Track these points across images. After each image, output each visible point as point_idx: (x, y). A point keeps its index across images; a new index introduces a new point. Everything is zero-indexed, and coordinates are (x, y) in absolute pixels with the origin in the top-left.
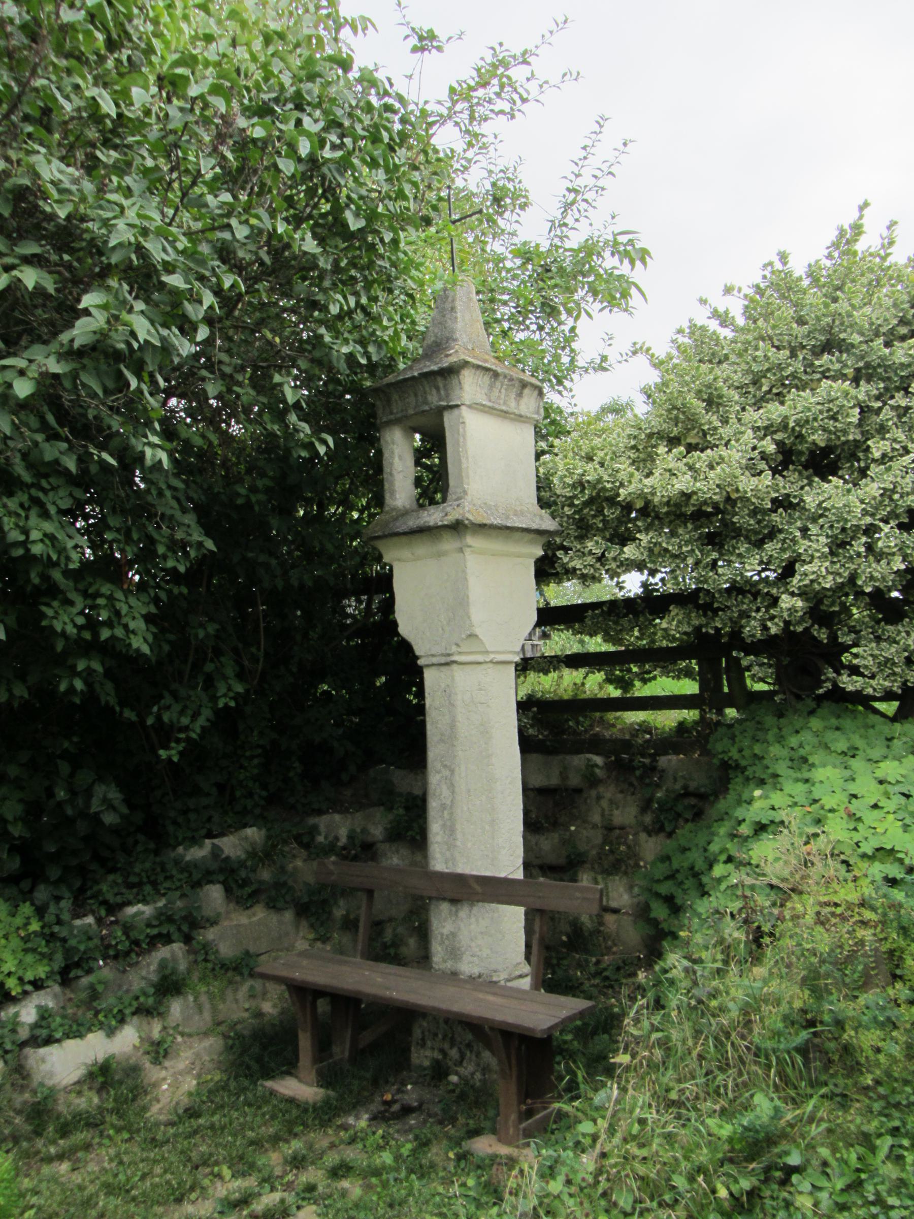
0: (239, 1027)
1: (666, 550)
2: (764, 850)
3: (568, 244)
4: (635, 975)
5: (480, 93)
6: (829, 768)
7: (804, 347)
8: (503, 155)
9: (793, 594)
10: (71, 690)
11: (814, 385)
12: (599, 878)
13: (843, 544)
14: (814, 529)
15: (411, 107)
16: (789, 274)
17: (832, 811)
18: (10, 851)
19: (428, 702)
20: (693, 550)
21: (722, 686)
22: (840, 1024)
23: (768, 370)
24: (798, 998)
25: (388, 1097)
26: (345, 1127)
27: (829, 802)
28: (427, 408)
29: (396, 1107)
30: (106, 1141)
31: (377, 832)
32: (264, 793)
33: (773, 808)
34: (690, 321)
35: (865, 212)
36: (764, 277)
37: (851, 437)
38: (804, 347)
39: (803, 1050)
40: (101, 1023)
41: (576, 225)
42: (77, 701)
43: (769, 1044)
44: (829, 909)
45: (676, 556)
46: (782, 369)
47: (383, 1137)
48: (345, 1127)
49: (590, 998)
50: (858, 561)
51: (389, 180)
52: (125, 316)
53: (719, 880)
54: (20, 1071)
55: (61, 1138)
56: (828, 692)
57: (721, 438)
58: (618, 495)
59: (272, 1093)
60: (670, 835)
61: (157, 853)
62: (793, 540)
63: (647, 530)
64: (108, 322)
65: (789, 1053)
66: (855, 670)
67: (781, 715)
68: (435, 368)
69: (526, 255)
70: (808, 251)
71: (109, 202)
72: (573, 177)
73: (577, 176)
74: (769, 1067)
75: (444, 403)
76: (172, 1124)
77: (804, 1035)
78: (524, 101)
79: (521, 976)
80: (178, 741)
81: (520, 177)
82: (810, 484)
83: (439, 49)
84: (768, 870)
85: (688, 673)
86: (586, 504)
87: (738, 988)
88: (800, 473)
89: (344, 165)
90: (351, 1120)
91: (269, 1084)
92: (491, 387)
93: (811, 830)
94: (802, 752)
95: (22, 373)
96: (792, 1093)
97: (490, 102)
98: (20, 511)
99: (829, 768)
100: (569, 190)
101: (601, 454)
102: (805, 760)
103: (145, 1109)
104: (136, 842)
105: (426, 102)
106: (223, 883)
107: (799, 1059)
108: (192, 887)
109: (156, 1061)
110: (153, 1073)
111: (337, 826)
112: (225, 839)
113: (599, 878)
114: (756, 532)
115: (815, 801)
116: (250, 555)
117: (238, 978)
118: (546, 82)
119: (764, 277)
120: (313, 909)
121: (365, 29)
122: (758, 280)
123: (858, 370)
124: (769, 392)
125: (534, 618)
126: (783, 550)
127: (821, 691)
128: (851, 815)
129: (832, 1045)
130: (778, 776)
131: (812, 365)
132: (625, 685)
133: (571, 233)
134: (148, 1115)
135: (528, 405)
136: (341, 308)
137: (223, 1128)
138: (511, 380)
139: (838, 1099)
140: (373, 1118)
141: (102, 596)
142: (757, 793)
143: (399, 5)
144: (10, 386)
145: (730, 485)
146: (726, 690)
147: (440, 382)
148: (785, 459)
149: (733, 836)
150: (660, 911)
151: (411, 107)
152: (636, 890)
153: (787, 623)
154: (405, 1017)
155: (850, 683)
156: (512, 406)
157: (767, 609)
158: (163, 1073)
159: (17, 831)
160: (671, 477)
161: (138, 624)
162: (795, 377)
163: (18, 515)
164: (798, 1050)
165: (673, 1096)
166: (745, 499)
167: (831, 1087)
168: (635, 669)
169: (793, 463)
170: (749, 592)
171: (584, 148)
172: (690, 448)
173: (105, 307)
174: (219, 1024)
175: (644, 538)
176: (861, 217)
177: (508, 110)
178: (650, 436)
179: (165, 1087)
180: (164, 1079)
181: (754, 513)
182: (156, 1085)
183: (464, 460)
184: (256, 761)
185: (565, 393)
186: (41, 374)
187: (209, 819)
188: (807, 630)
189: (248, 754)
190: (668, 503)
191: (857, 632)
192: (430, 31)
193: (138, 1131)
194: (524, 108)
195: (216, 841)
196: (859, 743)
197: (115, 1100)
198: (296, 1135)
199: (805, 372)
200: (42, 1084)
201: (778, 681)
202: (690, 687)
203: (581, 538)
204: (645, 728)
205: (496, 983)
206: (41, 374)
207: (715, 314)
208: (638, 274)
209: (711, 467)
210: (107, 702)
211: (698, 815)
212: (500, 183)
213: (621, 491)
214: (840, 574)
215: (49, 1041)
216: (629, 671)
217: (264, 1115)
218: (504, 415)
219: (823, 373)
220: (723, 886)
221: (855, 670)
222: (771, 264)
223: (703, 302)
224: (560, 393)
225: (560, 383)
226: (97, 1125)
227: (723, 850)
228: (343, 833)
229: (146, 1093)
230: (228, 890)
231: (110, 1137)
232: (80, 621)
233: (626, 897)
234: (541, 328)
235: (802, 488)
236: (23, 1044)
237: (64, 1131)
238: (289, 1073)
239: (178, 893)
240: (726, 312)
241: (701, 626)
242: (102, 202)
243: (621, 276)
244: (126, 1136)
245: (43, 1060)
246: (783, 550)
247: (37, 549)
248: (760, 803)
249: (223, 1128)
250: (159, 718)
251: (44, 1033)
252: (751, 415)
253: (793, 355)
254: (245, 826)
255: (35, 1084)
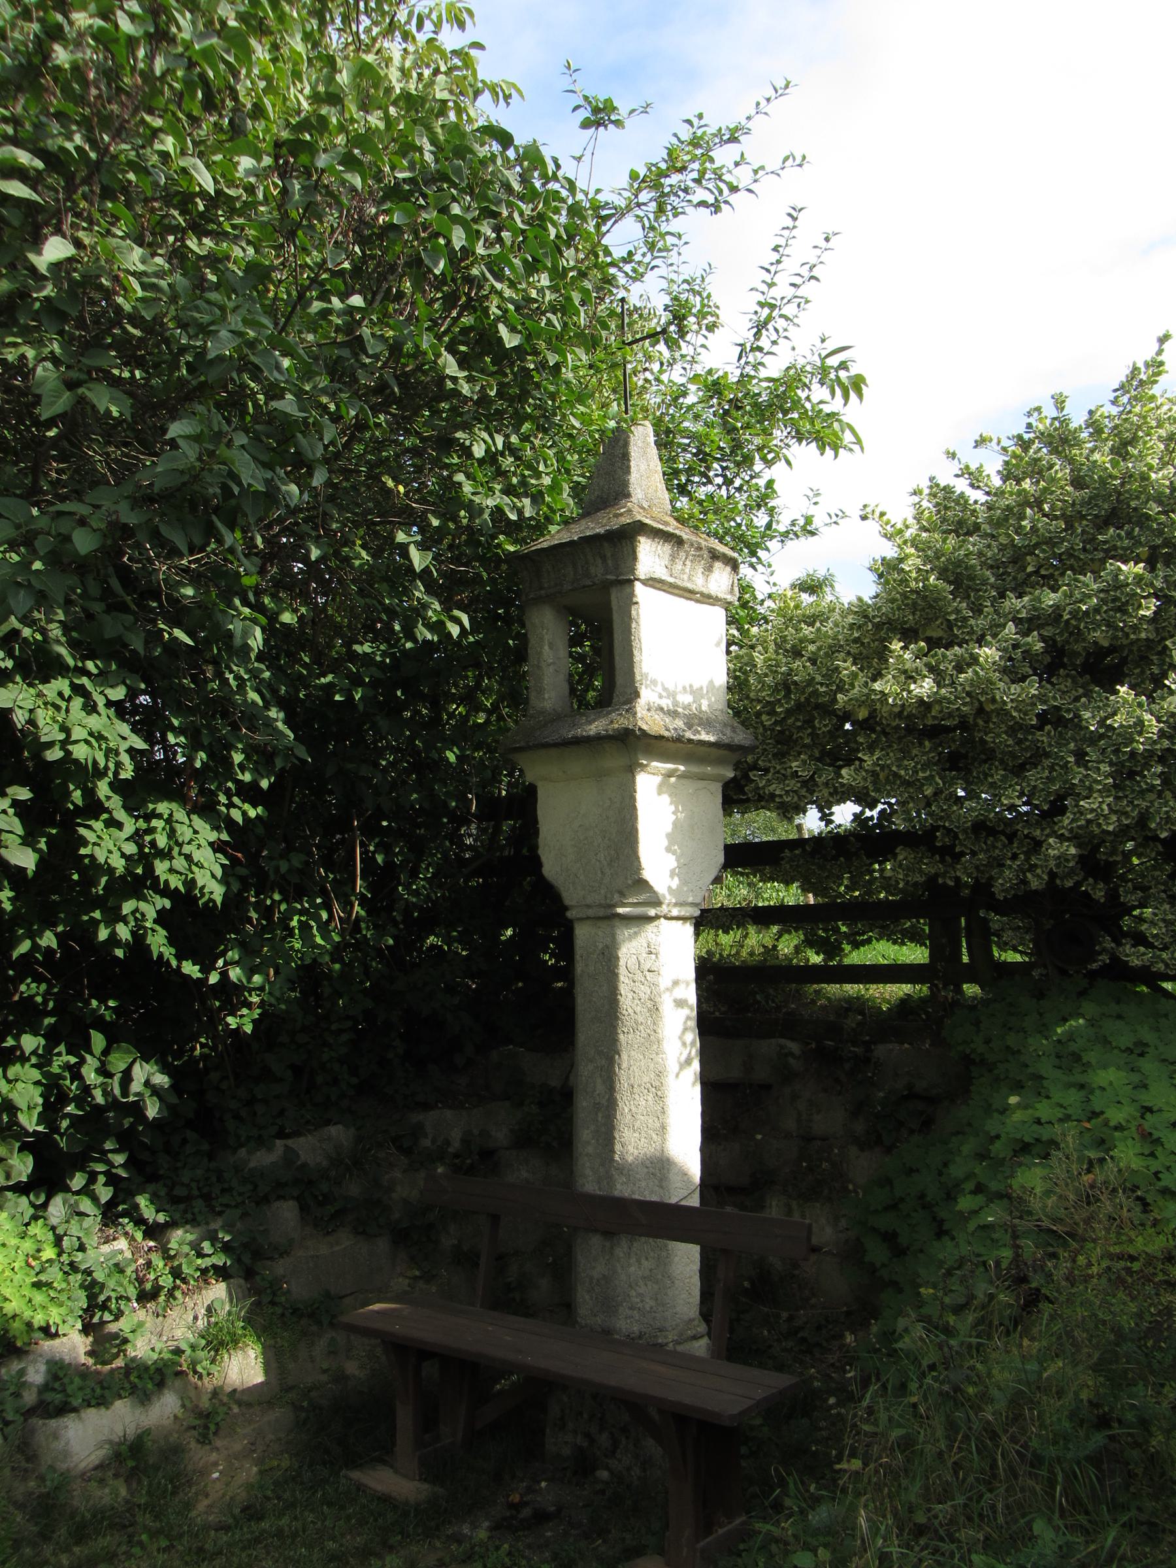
0: (313, 1394)
1: (896, 775)
2: (1031, 1178)
3: (763, 373)
4: (842, 1336)
5: (675, 179)
6: (1112, 1070)
7: (1083, 517)
8: (688, 261)
9: (1062, 838)
10: (113, 939)
11: (1096, 566)
12: (794, 1204)
13: (1132, 774)
14: (1093, 754)
15: (580, 196)
16: (1064, 422)
17: (1119, 1128)
18: (20, 1150)
19: (579, 967)
20: (932, 777)
21: (961, 954)
22: (1144, 1423)
23: (1037, 545)
24: (1086, 1385)
25: (515, 1498)
26: (458, 1539)
27: (1116, 1116)
28: (589, 583)
29: (526, 1512)
30: (136, 1550)
31: (500, 1136)
32: (354, 1081)
33: (1038, 1122)
34: (932, 479)
35: (1165, 346)
36: (1029, 426)
37: (1143, 635)
38: (1083, 517)
39: (1095, 1460)
40: (134, 1387)
41: (774, 349)
42: (119, 953)
43: (1052, 1451)
44: (1122, 1263)
45: (908, 784)
46: (1055, 545)
47: (509, 1554)
48: (458, 1539)
49: (780, 1368)
50: (1151, 796)
51: (554, 289)
52: (222, 451)
53: (964, 1218)
54: (26, 1450)
55: (77, 1544)
56: (1105, 967)
57: (972, 632)
58: (835, 701)
59: (360, 1487)
60: (889, 1150)
61: (211, 1156)
62: (1065, 766)
63: (871, 749)
64: (200, 459)
65: (1079, 1464)
66: (1140, 939)
67: (1040, 995)
68: (601, 531)
69: (714, 387)
70: (1090, 393)
71: (208, 302)
72: (764, 288)
73: (771, 285)
74: (1052, 1483)
75: (611, 577)
76: (226, 1528)
77: (1098, 1439)
78: (734, 189)
79: (695, 1338)
80: (249, 1006)
81: (709, 289)
82: (1088, 694)
83: (618, 123)
84: (1035, 1204)
85: (915, 937)
86: (789, 712)
87: (1005, 1367)
88: (1074, 682)
89: (495, 267)
90: (466, 1530)
91: (356, 1475)
92: (673, 558)
93: (1093, 1154)
94: (1073, 1047)
95: (82, 522)
96: (1082, 1519)
97: (686, 190)
98: (59, 702)
99: (1112, 1070)
100: (761, 305)
101: (812, 648)
102: (1076, 1057)
103: (188, 1506)
104: (185, 1141)
105: (598, 191)
106: (297, 1199)
107: (1092, 1471)
108: (258, 1203)
109: (204, 1440)
110: (199, 1455)
111: (448, 1126)
112: (302, 1140)
113: (794, 1204)
114: (1013, 755)
115: (1095, 1114)
116: (349, 766)
117: (314, 1328)
118: (762, 168)
119: (1029, 426)
120: (414, 1236)
121: (507, 97)
122: (1021, 429)
123: (1154, 549)
124: (1036, 572)
125: (721, 858)
126: (1050, 780)
127: (1095, 966)
128: (1146, 1136)
129: (1135, 1454)
130: (1042, 1078)
131: (1094, 539)
132: (831, 949)
133: (767, 360)
134: (193, 1514)
135: (720, 581)
136: (487, 451)
137: (295, 1535)
138: (699, 548)
139: (1144, 1528)
140: (495, 1527)
141: (160, 816)
142: (1013, 1100)
143: (569, 67)
144: (67, 539)
145: (984, 693)
146: (965, 959)
147: (607, 549)
148: (1052, 663)
149: (982, 1156)
150: (877, 1253)
151: (580, 196)
152: (843, 1223)
153: (1052, 875)
154: (540, 1388)
155: (1135, 956)
156: (698, 582)
157: (1028, 854)
158: (214, 1456)
159: (30, 1122)
160: (909, 680)
161: (205, 855)
162: (1071, 556)
163: (58, 708)
164: (1088, 1458)
165: (921, 1518)
166: (1002, 712)
167: (1133, 1513)
168: (844, 929)
169: (1064, 666)
170: (1003, 833)
171: (776, 249)
172: (933, 643)
173: (196, 438)
174: (289, 1389)
175: (869, 760)
176: (1160, 352)
177: (711, 200)
178: (878, 627)
179: (216, 1475)
180: (216, 1464)
181: (1014, 729)
182: (204, 1472)
183: (636, 652)
184: (344, 1037)
185: (759, 567)
186: (110, 524)
187: (282, 1113)
188: (1078, 884)
189: (334, 1027)
190: (899, 715)
191: (1144, 889)
192: (608, 101)
193: (181, 1536)
194: (733, 198)
195: (289, 1142)
196: (1148, 1036)
197: (149, 1493)
198: (391, 1548)
199: (1084, 549)
200: (52, 1468)
201: (1037, 952)
202: (915, 954)
203: (781, 756)
204: (856, 1005)
205: (661, 1345)
206: (110, 524)
207: (966, 472)
208: (852, 412)
209: (960, 669)
210: (161, 955)
211: (927, 1124)
212: (683, 297)
213: (839, 696)
214: (1126, 814)
215: (64, 1409)
216: (836, 930)
217: (349, 1518)
218: (688, 594)
219: (1106, 551)
220: (972, 1226)
221: (1140, 939)
222: (1038, 409)
223: (952, 455)
224: (752, 566)
225: (753, 554)
226: (124, 1527)
227: (970, 1176)
228: (456, 1136)
229: (190, 1483)
230: (304, 1208)
231: (141, 1544)
232: (131, 849)
233: (829, 1230)
234: (728, 482)
235: (1077, 699)
236: (30, 1412)
237: (81, 1533)
238: (382, 1461)
239: (239, 1212)
240: (980, 469)
241: (937, 875)
242: (199, 302)
243: (832, 415)
244: (164, 1543)
245: (56, 1436)
246: (1050, 780)
247: (80, 752)
248: (1017, 1113)
249: (295, 1535)
250: (224, 974)
251: (58, 1398)
252: (1012, 602)
253: (1070, 526)
254: (328, 1122)
255: (43, 1469)
